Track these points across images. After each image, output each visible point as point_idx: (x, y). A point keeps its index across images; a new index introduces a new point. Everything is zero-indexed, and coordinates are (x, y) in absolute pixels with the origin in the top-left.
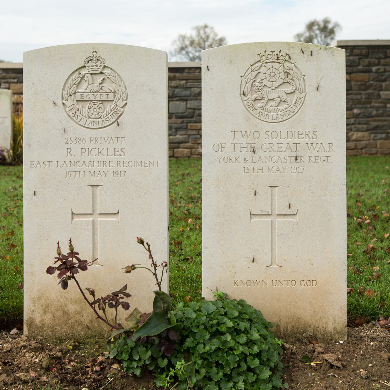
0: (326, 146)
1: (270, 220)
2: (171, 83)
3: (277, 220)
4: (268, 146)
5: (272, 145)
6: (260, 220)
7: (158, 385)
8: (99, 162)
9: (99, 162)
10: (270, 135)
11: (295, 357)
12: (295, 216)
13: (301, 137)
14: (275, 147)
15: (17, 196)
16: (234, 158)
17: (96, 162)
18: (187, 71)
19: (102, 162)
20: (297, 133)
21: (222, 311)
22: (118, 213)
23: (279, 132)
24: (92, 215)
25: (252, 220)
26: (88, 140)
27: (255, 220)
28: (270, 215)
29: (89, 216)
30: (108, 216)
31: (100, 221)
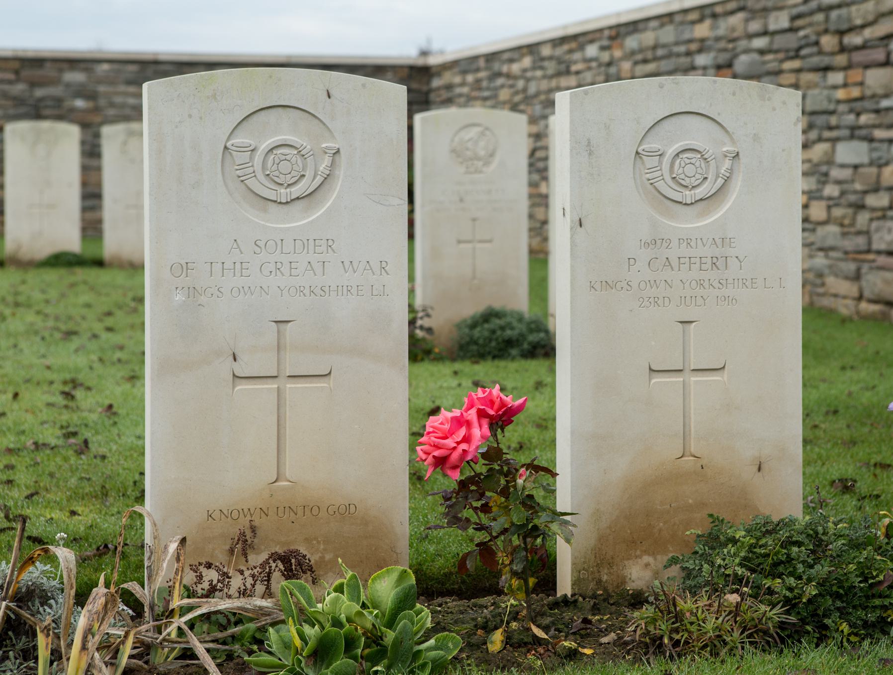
0: (376, 267)
1: (276, 386)
2: (826, 153)
3: (288, 386)
4: (272, 267)
6: (668, 380)
8: (340, 288)
10: (263, 247)
11: (657, 583)
14: (285, 269)
15: (121, 348)
16: (707, 282)
17: (333, 288)
20: (311, 242)
21: (800, 517)
22: (330, 373)
23: (279, 243)
25: (653, 381)
27: (657, 379)
29: (269, 380)
30: (265, 380)
31: (696, 382)
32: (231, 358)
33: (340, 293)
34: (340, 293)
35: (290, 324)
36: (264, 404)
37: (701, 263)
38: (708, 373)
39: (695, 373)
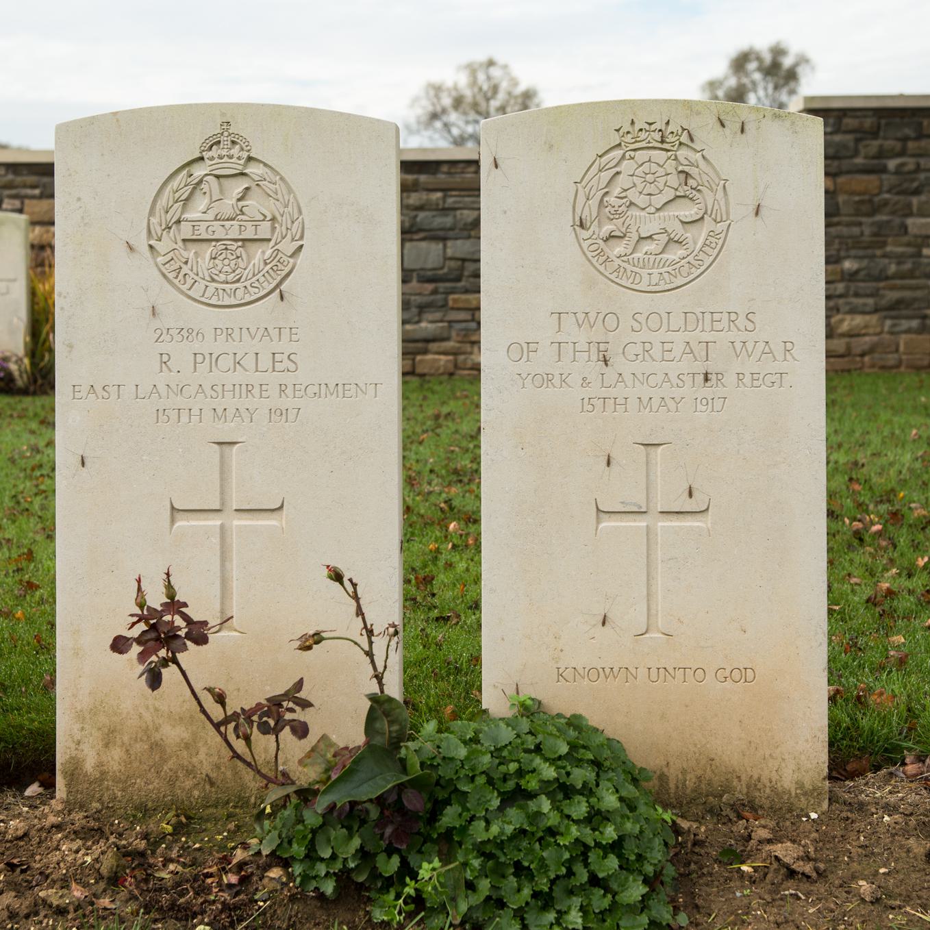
0: (778, 349)
1: (218, 523)
3: (660, 524)
4: (638, 349)
5: (648, 346)
8: (237, 387)
9: (237, 387)
10: (644, 322)
12: (279, 513)
14: (656, 352)
16: (557, 378)
17: (229, 387)
18: (445, 168)
19: (244, 387)
22: (281, 507)
24: (644, 515)
25: (601, 526)
27: (608, 524)
28: (645, 512)
29: (211, 515)
30: (199, 514)
32: (687, 493)
33: (237, 395)
34: (237, 395)
35: (662, 447)
36: (222, 540)
37: (291, 334)
38: (257, 514)
39: (239, 515)
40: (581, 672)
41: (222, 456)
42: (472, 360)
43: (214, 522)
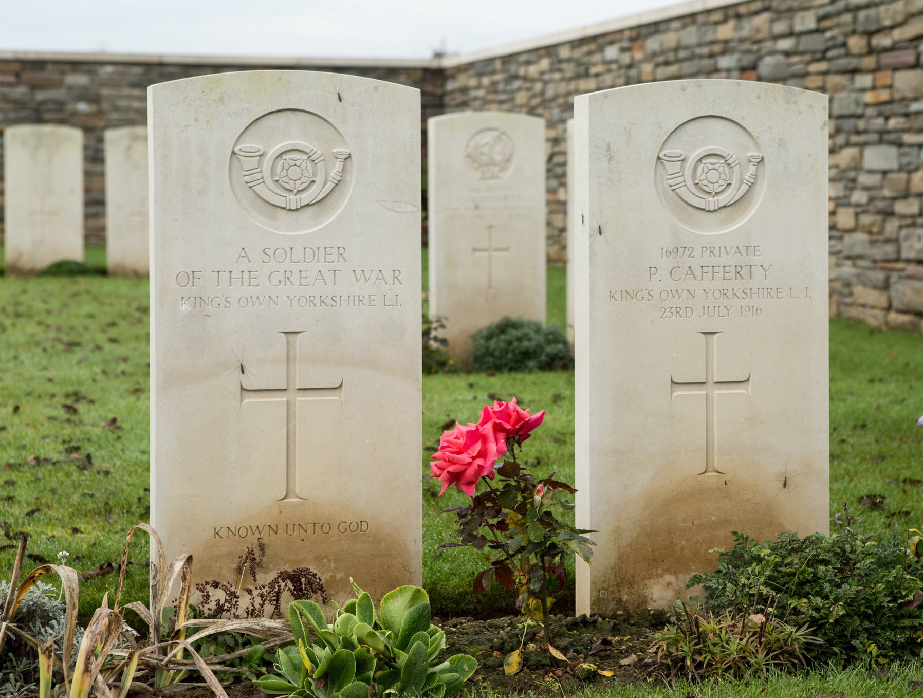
1: (285, 399)
4: (281, 276)
5: (288, 274)
7: (710, 543)
8: (352, 298)
9: (352, 298)
10: (272, 255)
12: (338, 391)
13: (329, 258)
14: (295, 278)
15: (125, 360)
16: (730, 292)
17: (345, 297)
18: (50, 67)
19: (357, 298)
22: (341, 386)
24: (284, 393)
25: (675, 394)
26: (697, 251)
27: (250, 399)
28: (285, 390)
29: (278, 393)
33: (351, 303)
34: (351, 303)
36: (273, 415)
40: (233, 530)
41: (288, 343)
42: (548, 319)
43: (282, 399)
